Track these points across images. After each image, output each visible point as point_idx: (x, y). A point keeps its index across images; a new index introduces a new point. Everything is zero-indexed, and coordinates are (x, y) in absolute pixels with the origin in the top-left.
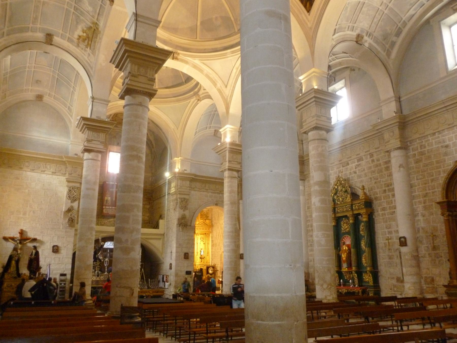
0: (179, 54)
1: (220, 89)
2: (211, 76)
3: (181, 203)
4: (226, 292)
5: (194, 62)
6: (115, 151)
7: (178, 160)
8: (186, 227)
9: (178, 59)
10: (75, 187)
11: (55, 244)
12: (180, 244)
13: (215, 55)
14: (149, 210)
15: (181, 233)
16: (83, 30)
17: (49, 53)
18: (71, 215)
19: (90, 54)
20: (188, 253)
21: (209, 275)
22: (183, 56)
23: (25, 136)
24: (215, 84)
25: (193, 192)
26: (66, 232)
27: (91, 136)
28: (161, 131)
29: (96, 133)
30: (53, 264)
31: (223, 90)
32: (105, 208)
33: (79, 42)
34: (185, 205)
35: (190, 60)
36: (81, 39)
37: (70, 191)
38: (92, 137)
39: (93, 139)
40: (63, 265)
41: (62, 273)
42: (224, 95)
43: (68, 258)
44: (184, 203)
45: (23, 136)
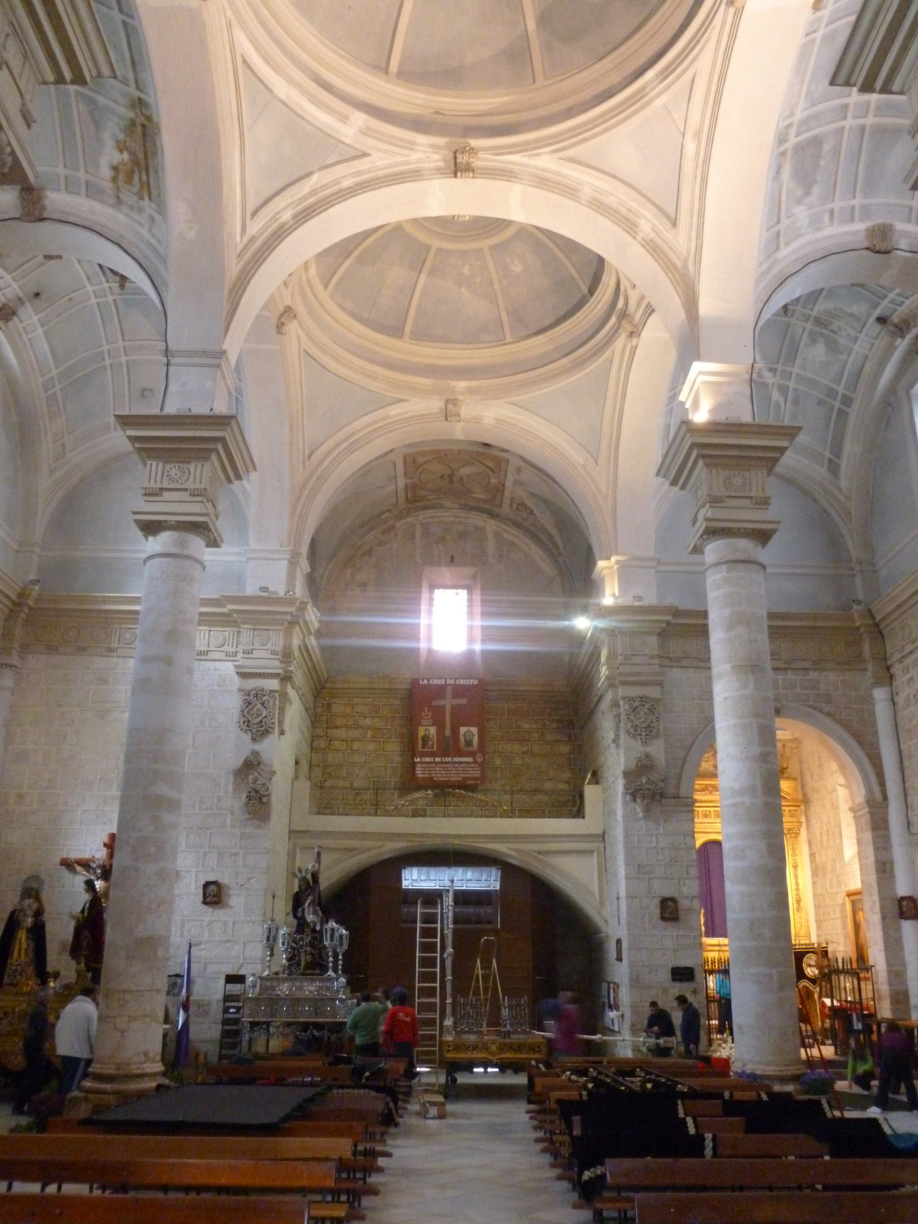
0: (473, 151)
1: (652, 241)
2: (612, 201)
3: (632, 717)
4: (744, 1065)
5: (536, 168)
6: (449, 583)
7: (611, 568)
8: (660, 802)
9: (473, 171)
10: (262, 690)
11: (211, 878)
12: (639, 866)
13: (604, 114)
14: (569, 759)
15: (642, 822)
16: (118, 142)
17: (60, 257)
18: (256, 780)
19: (156, 216)
20: (673, 900)
21: (804, 983)
22: (493, 157)
23: (126, 555)
24: (629, 225)
25: (676, 674)
26: (243, 836)
27: (159, 478)
28: (560, 491)
29: (177, 465)
30: (207, 942)
31: (664, 241)
32: (421, 763)
33: (118, 189)
34: (648, 722)
35: (521, 164)
36: (121, 177)
37: (250, 703)
38: (161, 483)
39: (165, 485)
40: (237, 947)
41: (232, 973)
42: (673, 257)
43: (253, 922)
44: (642, 713)
45: (118, 555)
